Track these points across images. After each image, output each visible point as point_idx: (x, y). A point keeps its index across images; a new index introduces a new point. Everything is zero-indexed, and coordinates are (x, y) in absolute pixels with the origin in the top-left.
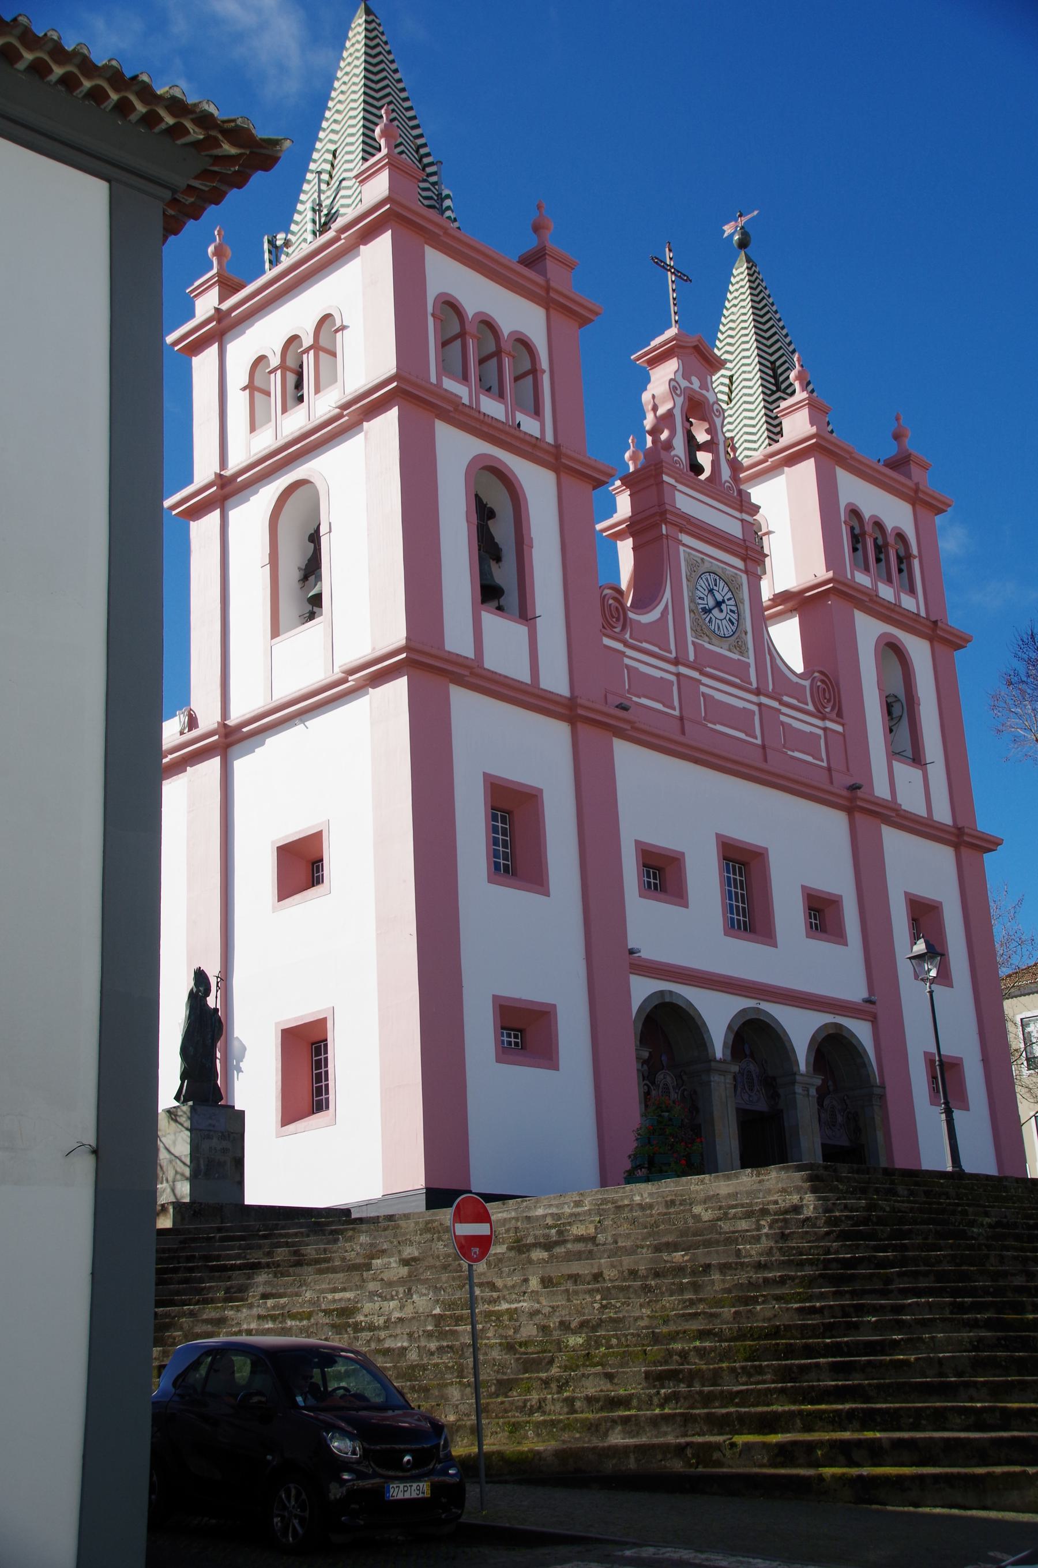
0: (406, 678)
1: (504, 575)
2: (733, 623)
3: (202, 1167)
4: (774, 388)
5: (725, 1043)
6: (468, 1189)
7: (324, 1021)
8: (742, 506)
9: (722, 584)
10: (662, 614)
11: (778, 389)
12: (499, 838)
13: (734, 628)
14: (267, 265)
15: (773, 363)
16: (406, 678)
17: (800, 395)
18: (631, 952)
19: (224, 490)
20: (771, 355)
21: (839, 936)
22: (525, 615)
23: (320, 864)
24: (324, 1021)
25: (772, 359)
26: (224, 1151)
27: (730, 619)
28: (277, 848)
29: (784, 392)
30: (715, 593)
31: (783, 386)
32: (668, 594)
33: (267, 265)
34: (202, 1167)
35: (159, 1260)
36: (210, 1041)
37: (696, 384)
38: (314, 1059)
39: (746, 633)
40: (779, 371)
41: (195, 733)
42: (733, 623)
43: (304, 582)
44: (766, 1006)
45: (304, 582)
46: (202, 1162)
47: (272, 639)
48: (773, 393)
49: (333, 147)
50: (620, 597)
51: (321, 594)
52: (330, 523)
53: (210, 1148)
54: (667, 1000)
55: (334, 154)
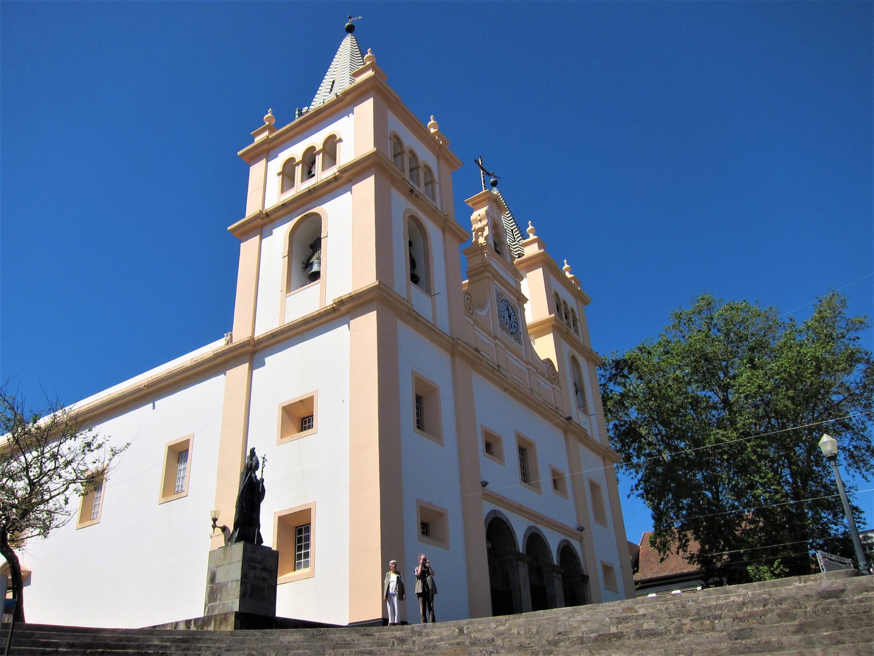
0: (375, 312)
1: (419, 272)
3: (249, 589)
4: (514, 240)
5: (523, 544)
7: (309, 511)
8: (516, 274)
10: (487, 313)
14: (297, 116)
15: (512, 230)
16: (375, 312)
17: (532, 237)
18: (484, 484)
19: (263, 221)
20: (511, 227)
21: (564, 494)
22: (428, 291)
23: (311, 418)
24: (309, 511)
25: (512, 228)
26: (264, 579)
28: (282, 407)
32: (489, 305)
33: (297, 116)
34: (249, 589)
37: (496, 216)
39: (521, 334)
41: (231, 345)
43: (305, 269)
44: (539, 526)
45: (305, 269)
46: (248, 585)
47: (286, 293)
48: (513, 242)
50: (470, 298)
51: (320, 272)
53: (255, 576)
55: (333, 82)
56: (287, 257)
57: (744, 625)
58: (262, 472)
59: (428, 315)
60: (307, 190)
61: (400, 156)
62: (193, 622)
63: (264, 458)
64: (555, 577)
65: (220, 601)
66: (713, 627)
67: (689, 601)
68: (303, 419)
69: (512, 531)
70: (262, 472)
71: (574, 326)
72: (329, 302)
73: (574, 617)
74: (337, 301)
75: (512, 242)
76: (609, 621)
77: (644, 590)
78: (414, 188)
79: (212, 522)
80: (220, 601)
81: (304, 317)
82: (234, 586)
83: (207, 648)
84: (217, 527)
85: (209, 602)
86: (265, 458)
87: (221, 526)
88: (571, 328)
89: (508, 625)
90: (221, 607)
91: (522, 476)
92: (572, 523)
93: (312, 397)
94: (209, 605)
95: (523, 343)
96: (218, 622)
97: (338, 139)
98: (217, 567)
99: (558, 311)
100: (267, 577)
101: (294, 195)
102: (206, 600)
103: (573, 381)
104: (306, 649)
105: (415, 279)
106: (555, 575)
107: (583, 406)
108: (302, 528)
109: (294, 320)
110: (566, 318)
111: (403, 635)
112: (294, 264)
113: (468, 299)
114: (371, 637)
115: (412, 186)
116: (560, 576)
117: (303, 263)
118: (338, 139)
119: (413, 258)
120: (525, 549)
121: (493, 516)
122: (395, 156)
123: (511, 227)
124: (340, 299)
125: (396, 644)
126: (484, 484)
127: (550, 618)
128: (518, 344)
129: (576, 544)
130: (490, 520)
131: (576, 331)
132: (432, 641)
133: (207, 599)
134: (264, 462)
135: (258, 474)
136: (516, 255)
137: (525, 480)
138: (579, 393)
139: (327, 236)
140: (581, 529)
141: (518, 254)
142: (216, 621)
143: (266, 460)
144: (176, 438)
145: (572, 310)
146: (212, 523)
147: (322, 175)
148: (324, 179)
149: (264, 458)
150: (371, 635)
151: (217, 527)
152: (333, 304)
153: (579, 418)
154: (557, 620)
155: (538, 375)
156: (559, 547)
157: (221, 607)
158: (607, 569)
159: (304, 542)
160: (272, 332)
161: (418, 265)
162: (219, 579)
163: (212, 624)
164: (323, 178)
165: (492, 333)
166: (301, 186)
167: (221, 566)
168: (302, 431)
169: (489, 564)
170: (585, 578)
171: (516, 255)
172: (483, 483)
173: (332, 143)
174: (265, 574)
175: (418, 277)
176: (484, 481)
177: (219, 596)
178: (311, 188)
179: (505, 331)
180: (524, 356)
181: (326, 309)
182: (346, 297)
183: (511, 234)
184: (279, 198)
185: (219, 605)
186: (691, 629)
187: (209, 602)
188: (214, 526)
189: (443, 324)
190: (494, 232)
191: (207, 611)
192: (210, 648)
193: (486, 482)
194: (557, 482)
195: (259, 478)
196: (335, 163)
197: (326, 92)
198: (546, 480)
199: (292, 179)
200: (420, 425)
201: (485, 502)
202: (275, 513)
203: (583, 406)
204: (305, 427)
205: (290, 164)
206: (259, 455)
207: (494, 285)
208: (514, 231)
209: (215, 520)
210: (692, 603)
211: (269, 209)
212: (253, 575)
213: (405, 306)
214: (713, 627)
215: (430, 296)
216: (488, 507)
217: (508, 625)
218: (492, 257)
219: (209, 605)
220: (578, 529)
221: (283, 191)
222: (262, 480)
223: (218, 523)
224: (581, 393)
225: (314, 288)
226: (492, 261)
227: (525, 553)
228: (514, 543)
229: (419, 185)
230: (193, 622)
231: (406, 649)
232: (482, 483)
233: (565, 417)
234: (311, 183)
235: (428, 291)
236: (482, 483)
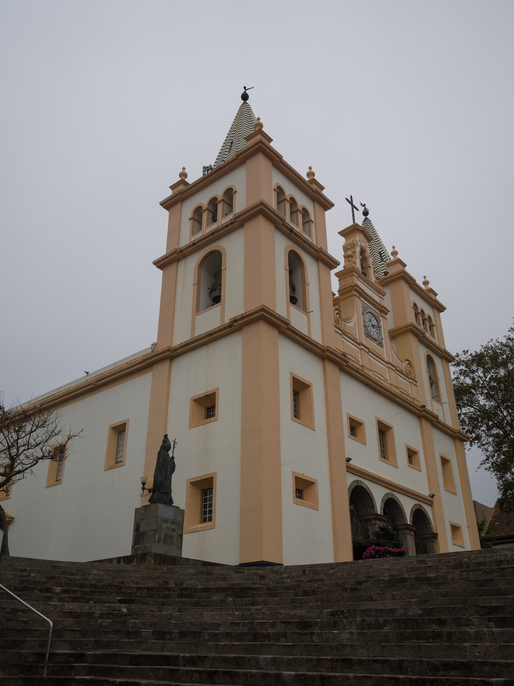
1: (299, 295)
2: (378, 334)
4: (381, 261)
5: (381, 509)
6: (282, 563)
9: (374, 318)
11: (382, 261)
12: (209, 497)
13: (378, 336)
15: (380, 252)
18: (348, 460)
20: (379, 250)
22: (305, 310)
25: (380, 251)
26: (174, 530)
27: (377, 333)
29: (384, 262)
30: (372, 321)
31: (384, 260)
35: (212, 490)
36: (169, 473)
38: (203, 504)
39: (382, 339)
40: (382, 255)
42: (378, 334)
46: (162, 534)
47: (196, 313)
48: (381, 262)
49: (231, 141)
51: (221, 296)
52: (253, 88)
53: (167, 527)
54: (360, 485)
55: (232, 143)
56: (197, 285)
57: (489, 577)
58: (173, 451)
59: (302, 329)
60: (211, 233)
61: (282, 203)
62: (122, 559)
63: (174, 442)
64: (408, 533)
65: (142, 545)
66: (468, 577)
67: (464, 558)
68: (208, 409)
69: (371, 497)
70: (173, 451)
71: (430, 330)
72: (227, 321)
73: (383, 566)
74: (232, 320)
75: (379, 263)
76: (405, 569)
77: (505, 545)
78: (293, 228)
79: (142, 485)
80: (142, 545)
81: (208, 332)
82: (152, 534)
83: (129, 577)
84: (145, 489)
85: (135, 545)
86: (175, 441)
87: (148, 488)
88: (427, 332)
89: (336, 569)
90: (143, 549)
91: (382, 453)
92: (425, 492)
93: (215, 392)
94: (135, 547)
95: (384, 346)
96: (139, 559)
97: (234, 191)
98: (140, 520)
99: (416, 318)
100: (175, 528)
101: (201, 237)
102: (133, 544)
103: (428, 375)
104: (196, 581)
105: (293, 300)
106: (408, 532)
107: (437, 397)
108: (207, 491)
109: (201, 334)
110: (423, 324)
111: (264, 573)
112: (202, 290)
113: (337, 314)
114: (242, 574)
115: (292, 227)
116: (413, 533)
117: (209, 288)
118: (234, 191)
119: (293, 284)
120: (382, 511)
121: (355, 485)
122: (278, 203)
123: (379, 250)
124: (235, 319)
125: (258, 579)
126: (348, 460)
127: (366, 566)
128: (380, 348)
129: (428, 509)
130: (353, 488)
131: (432, 334)
132: (283, 578)
133: (134, 543)
134: (174, 444)
135: (170, 453)
136: (382, 273)
137: (384, 456)
138: (434, 385)
139: (226, 269)
140: (433, 496)
141: (384, 272)
142: (137, 558)
143: (176, 443)
144: (117, 421)
145: (429, 317)
146: (142, 486)
147: (222, 220)
148: (224, 224)
149: (174, 442)
150: (242, 573)
151: (145, 489)
152: (229, 323)
153: (433, 407)
154: (371, 567)
155: (397, 372)
156: (412, 509)
157: (143, 549)
158: (455, 529)
159: (209, 502)
160: (185, 343)
161: (296, 289)
162: (142, 529)
163: (135, 561)
164: (223, 223)
165: (357, 340)
166: (207, 229)
167: (143, 520)
168: (208, 418)
169: (352, 521)
170: (435, 536)
171: (382, 273)
172: (347, 459)
173: (230, 193)
174: (174, 526)
175: (296, 299)
176: (348, 458)
177: (141, 541)
178: (213, 231)
179: (369, 338)
180: (386, 358)
181: (225, 326)
182: (239, 317)
183: (379, 255)
184: (190, 239)
185: (141, 548)
186: (453, 578)
187: (135, 545)
188: (143, 489)
189: (317, 337)
190: (361, 257)
191: (133, 551)
192: (131, 578)
193: (350, 458)
194: (411, 454)
195: (171, 456)
196: (232, 212)
197: (226, 152)
198: (402, 456)
199: (200, 223)
200: (297, 414)
201: (348, 474)
202: (187, 479)
203: (437, 397)
204: (210, 415)
205: (198, 211)
206: (171, 439)
207: (360, 302)
208: (381, 253)
209: (144, 484)
210: (467, 560)
211: (183, 247)
212: (165, 527)
213: (285, 323)
214: (468, 577)
215: (305, 313)
216: (351, 479)
217: (337, 569)
218: (359, 278)
219: (135, 547)
220: (429, 496)
221: (193, 233)
222: (173, 458)
223: (146, 486)
224: (435, 385)
225: (217, 309)
226: (359, 281)
227: (383, 514)
228: (372, 505)
229: (297, 225)
230: (122, 559)
231: (264, 583)
232: (346, 459)
233: (420, 406)
234: (214, 227)
235: (305, 310)
236: (346, 459)
